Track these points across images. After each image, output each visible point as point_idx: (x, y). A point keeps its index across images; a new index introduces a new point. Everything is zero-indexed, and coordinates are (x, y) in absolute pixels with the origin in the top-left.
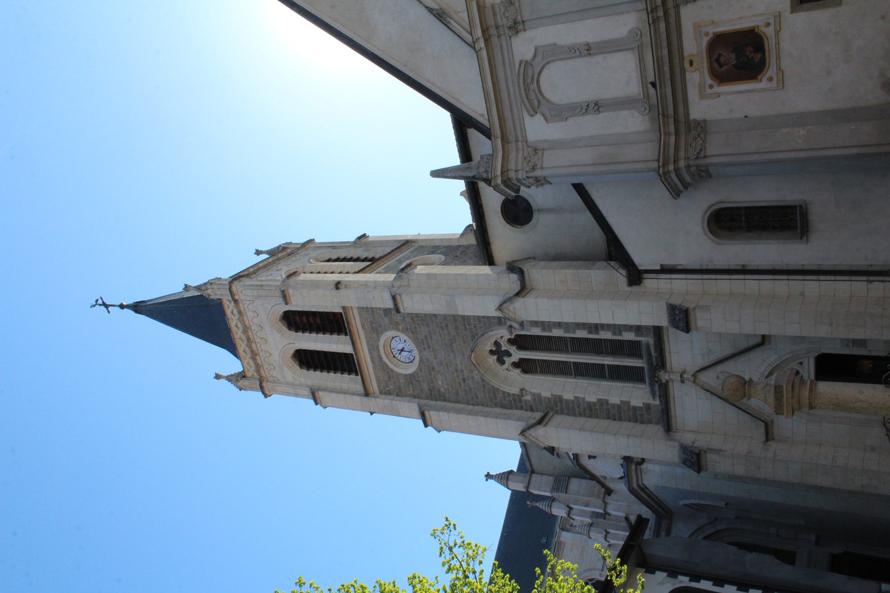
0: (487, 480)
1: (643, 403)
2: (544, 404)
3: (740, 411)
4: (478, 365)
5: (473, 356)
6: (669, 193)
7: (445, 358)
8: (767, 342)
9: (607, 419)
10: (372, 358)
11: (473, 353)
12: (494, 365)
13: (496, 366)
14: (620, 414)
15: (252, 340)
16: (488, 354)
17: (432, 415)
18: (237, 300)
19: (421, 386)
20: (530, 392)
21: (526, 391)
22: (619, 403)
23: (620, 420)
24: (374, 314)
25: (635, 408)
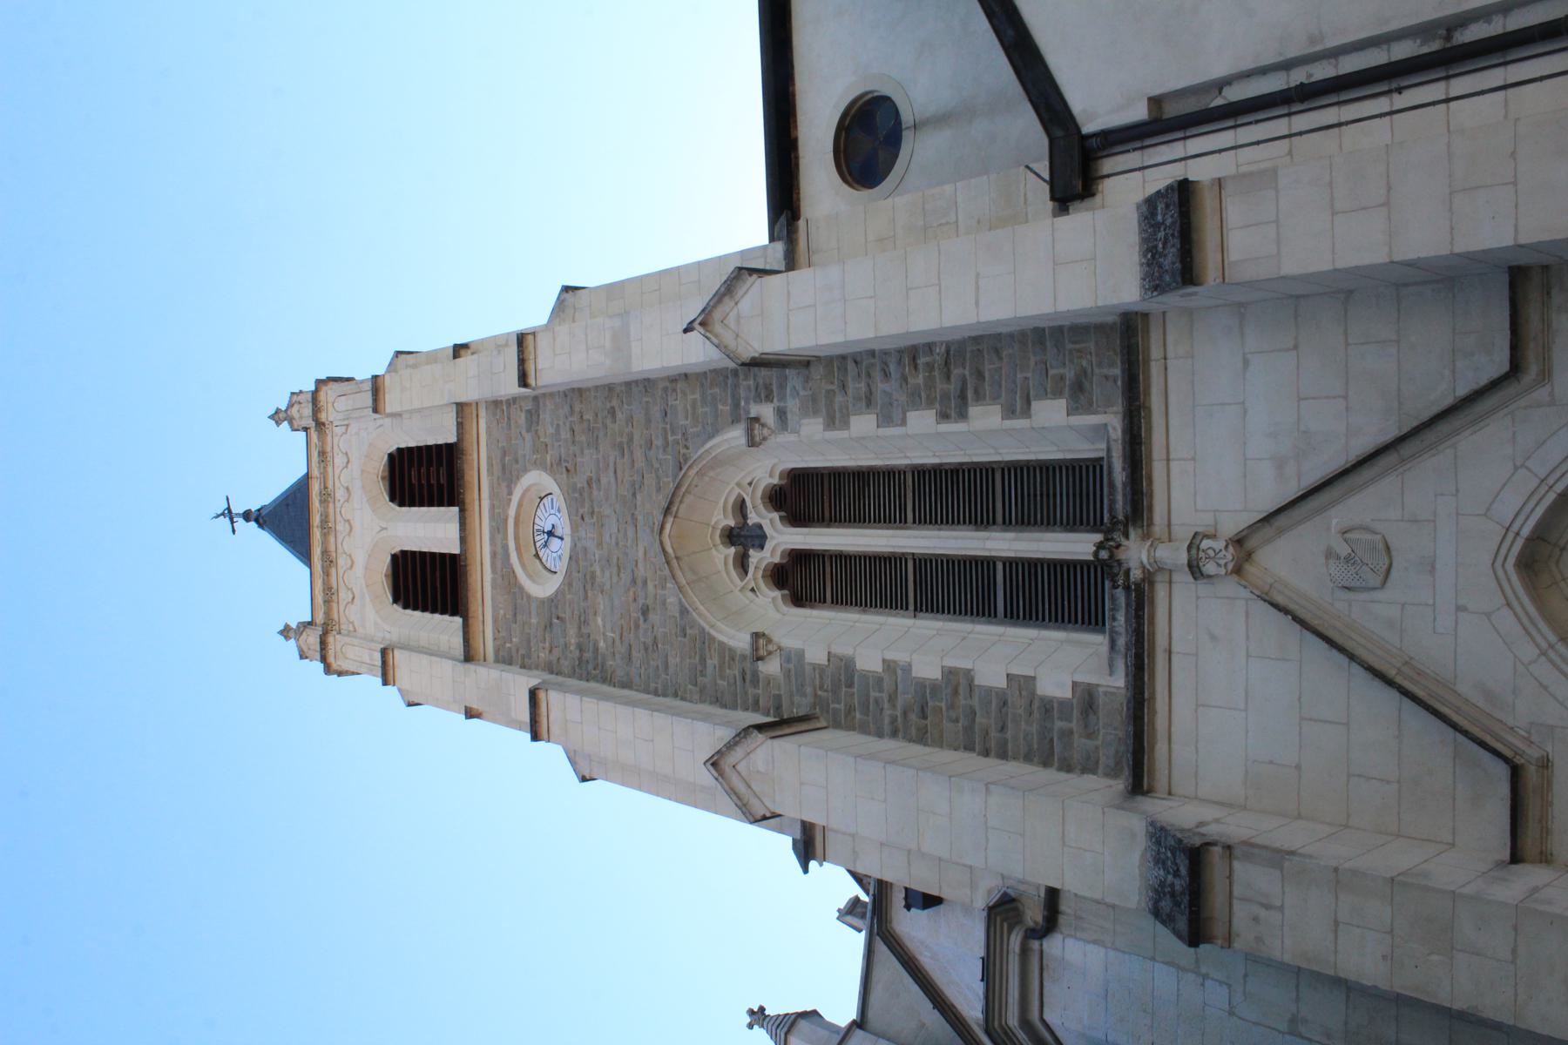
0: (750, 1026)
1: (1075, 684)
2: (809, 690)
3: (1407, 703)
4: (677, 558)
5: (668, 527)
6: (1496, 548)
7: (617, 544)
8: (1533, 370)
9: (966, 748)
10: (494, 555)
11: (670, 519)
12: (725, 575)
13: (728, 573)
14: (1003, 729)
15: (330, 525)
16: (718, 540)
17: (558, 704)
18: (324, 424)
19: (565, 637)
20: (780, 648)
21: (769, 641)
22: (1003, 684)
23: (1003, 755)
24: (510, 429)
25: (1048, 706)
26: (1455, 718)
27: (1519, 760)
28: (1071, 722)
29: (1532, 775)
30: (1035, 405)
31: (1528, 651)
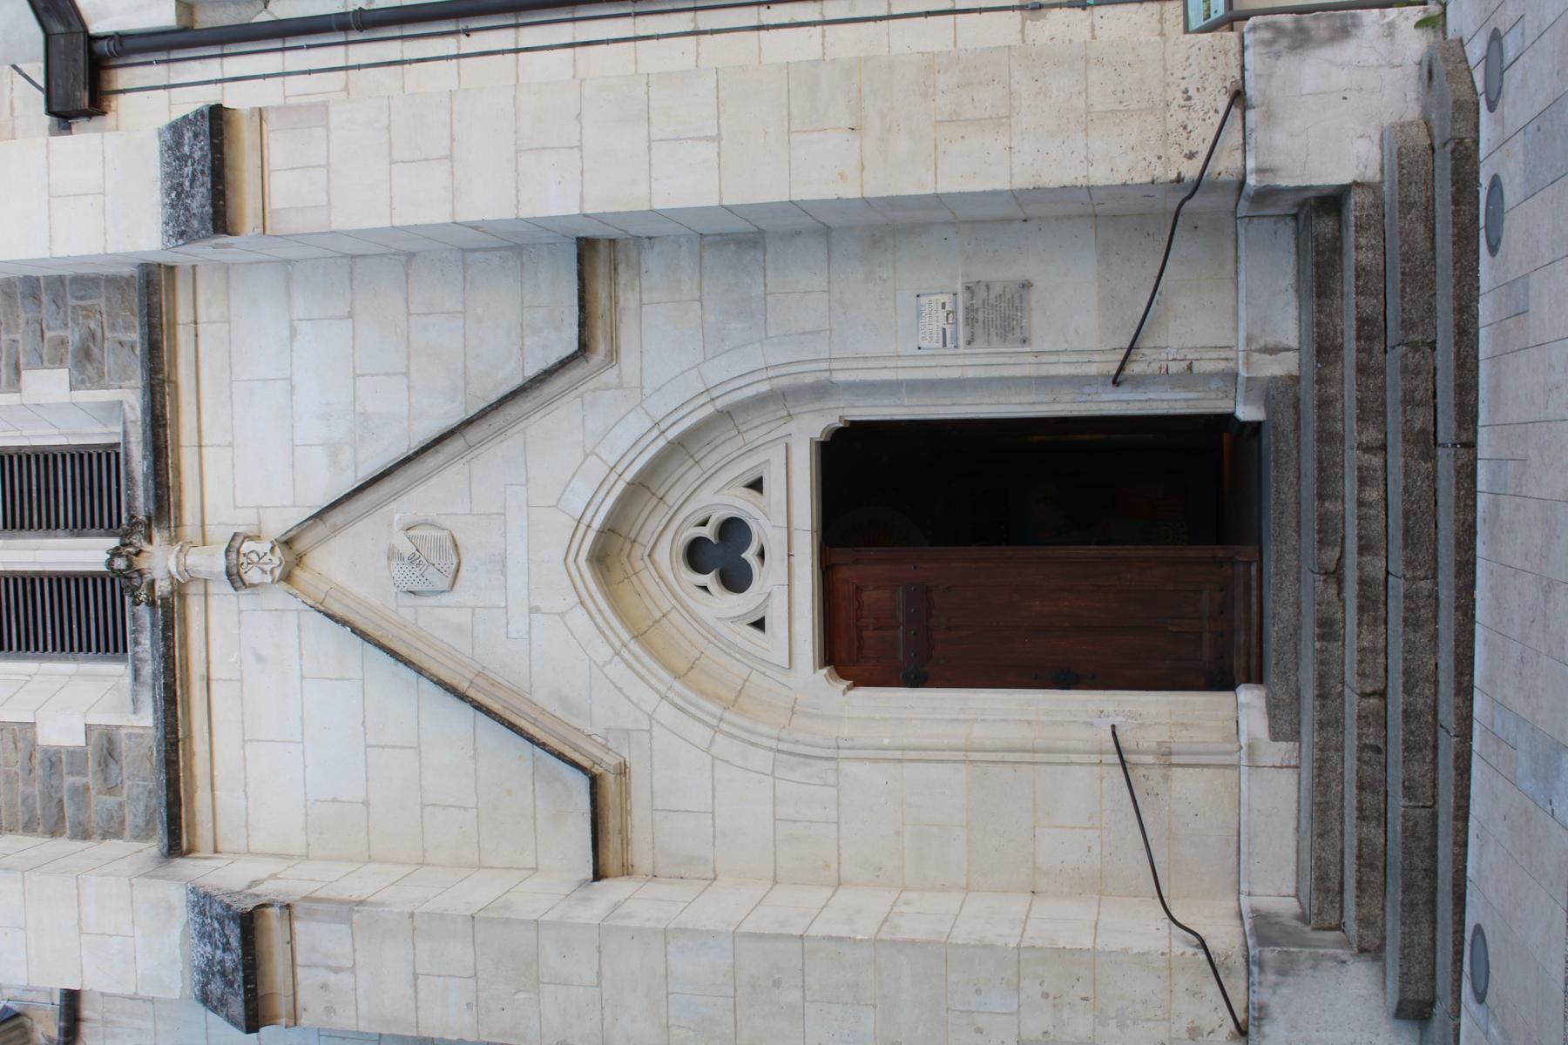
1: (88, 727)
8: (601, 348)
26: (532, 730)
27: (597, 770)
28: (85, 775)
29: (610, 784)
30: (25, 374)
31: (603, 652)
